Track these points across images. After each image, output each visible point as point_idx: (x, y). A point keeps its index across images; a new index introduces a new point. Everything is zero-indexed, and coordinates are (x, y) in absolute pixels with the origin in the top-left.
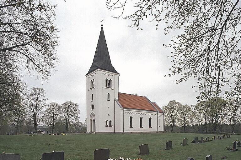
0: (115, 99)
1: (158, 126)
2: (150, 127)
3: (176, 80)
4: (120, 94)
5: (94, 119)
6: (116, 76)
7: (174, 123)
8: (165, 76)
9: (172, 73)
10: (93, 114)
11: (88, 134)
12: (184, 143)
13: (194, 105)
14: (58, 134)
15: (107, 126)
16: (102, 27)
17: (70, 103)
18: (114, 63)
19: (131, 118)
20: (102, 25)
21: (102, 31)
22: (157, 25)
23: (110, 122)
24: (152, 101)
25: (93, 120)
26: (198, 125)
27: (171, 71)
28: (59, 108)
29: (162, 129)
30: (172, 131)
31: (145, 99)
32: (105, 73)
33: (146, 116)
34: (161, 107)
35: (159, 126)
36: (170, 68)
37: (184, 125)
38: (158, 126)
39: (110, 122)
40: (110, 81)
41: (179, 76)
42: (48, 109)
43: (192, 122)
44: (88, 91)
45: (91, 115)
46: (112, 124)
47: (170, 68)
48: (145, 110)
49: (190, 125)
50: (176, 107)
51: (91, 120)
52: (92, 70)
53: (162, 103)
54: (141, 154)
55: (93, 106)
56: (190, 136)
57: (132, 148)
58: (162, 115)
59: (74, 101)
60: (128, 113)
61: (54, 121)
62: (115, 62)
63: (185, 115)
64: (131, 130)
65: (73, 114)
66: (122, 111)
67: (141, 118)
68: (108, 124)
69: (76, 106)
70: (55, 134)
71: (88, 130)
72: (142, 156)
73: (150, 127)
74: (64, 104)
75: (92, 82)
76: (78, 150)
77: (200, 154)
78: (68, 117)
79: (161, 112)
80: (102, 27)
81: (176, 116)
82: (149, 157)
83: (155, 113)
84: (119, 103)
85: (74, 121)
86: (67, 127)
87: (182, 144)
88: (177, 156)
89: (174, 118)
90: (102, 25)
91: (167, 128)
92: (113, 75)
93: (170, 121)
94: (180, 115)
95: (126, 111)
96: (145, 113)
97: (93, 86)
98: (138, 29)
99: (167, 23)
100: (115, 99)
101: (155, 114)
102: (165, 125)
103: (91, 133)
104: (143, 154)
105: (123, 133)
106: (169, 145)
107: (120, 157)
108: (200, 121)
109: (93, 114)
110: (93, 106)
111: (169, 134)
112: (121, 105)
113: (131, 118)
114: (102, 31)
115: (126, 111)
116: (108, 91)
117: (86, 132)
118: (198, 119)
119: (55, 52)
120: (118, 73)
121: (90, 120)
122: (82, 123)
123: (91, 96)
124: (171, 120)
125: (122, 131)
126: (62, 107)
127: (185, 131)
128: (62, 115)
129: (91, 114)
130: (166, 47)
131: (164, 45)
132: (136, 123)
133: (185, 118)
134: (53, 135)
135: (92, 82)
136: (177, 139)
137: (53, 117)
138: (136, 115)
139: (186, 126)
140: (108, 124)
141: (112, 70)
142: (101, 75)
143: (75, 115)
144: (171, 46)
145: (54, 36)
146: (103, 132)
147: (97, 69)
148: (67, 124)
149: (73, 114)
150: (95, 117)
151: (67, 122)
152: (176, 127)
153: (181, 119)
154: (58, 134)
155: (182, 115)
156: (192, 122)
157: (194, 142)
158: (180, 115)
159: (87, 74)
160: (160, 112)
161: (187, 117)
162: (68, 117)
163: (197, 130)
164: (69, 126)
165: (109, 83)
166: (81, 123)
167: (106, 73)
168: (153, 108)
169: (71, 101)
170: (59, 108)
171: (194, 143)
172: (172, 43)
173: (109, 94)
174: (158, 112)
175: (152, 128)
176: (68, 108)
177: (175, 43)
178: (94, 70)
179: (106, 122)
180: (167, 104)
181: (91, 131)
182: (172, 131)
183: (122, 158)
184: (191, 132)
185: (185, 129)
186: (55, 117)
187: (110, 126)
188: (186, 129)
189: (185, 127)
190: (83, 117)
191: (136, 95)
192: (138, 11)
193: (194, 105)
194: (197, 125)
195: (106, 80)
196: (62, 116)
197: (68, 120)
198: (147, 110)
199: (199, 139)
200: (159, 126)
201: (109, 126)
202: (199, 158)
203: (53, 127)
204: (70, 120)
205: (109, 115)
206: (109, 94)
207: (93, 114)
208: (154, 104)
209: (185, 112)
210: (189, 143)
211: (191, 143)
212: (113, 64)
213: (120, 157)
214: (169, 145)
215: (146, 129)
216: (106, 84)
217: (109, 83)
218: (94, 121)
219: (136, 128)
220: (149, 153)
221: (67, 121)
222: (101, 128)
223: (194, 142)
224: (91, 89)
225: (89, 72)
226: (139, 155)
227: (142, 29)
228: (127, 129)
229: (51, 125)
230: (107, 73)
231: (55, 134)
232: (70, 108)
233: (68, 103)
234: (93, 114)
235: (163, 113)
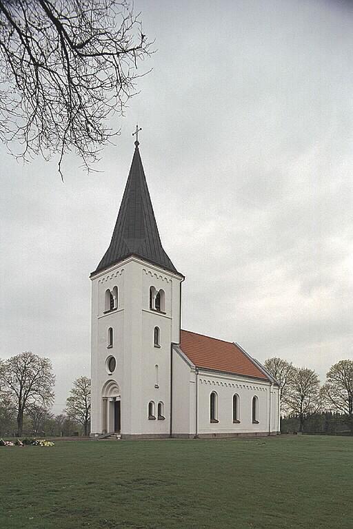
5: (115, 398)
6: (176, 282)
10: (112, 384)
15: (151, 418)
16: (137, 149)
17: (28, 357)
18: (169, 244)
20: (137, 143)
32: (148, 270)
39: (159, 405)
44: (96, 320)
45: (104, 387)
46: (166, 413)
51: (105, 399)
52: (109, 261)
59: (41, 355)
62: (171, 240)
64: (237, 429)
68: (155, 413)
69: (44, 364)
71: (96, 428)
75: (111, 298)
80: (137, 149)
83: (265, 386)
84: (180, 351)
90: (137, 143)
92: (169, 278)
95: (204, 377)
100: (172, 344)
102: (281, 417)
103: (105, 436)
105: (196, 437)
115: (203, 378)
116: (156, 319)
125: (192, 432)
126: (8, 366)
132: (224, 409)
134: (12, 444)
135: (111, 298)
138: (226, 387)
140: (155, 413)
141: (165, 264)
159: (93, 274)
164: (28, 419)
165: (157, 300)
169: (33, 353)
174: (271, 383)
179: (150, 405)
181: (106, 431)
187: (161, 418)
197: (25, 400)
198: (239, 375)
201: (157, 417)
204: (31, 400)
206: (157, 329)
212: (166, 246)
215: (246, 427)
216: (151, 305)
217: (157, 300)
218: (117, 405)
219: (225, 426)
222: (136, 424)
224: (105, 313)
225: (101, 268)
228: (206, 428)
230: (153, 272)
231: (17, 444)
233: (25, 356)
234: (114, 386)
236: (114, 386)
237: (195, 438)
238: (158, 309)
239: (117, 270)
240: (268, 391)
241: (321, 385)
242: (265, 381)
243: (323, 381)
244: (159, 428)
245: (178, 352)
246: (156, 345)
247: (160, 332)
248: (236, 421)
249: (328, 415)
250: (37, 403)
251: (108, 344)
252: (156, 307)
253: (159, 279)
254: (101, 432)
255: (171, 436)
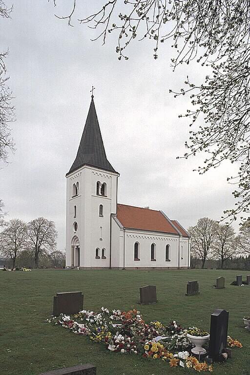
0: (111, 214)
1: (180, 258)
2: (167, 259)
3: (199, 167)
4: (119, 206)
5: (78, 246)
6: (114, 177)
7: (206, 254)
8: (178, 158)
9: (189, 151)
11: (68, 270)
12: (219, 285)
13: (230, 211)
14: (17, 269)
15: (97, 257)
16: (92, 100)
17: (42, 221)
19: (136, 245)
20: (93, 97)
21: (92, 105)
22: (156, 50)
23: (103, 250)
24: (171, 218)
25: (76, 247)
26: (245, 257)
27: (188, 147)
28: (25, 229)
29: (186, 263)
30: (203, 266)
31: (159, 214)
33: (161, 241)
34: (186, 228)
35: (182, 259)
36: (186, 142)
37: (222, 256)
38: (180, 258)
39: (103, 250)
40: (104, 186)
41: (203, 156)
42: (7, 231)
43: (234, 253)
44: (68, 201)
45: (72, 240)
46: (107, 254)
47: (186, 142)
48: (159, 232)
49: (232, 258)
50: (209, 229)
51: (73, 247)
52: (74, 169)
53: (187, 224)
54: (141, 302)
55: (76, 224)
56: (230, 275)
57: (129, 293)
58: (176, 238)
59: (49, 218)
60: (133, 237)
61: (15, 250)
63: (224, 241)
64: (137, 264)
65: (47, 238)
66: (122, 233)
67: (153, 246)
68: (100, 255)
70: (12, 270)
71: (68, 264)
72: (143, 307)
73: (167, 259)
74: (33, 223)
75: (76, 187)
76: (37, 294)
77: (243, 303)
78: (38, 243)
79: (186, 236)
80: (92, 100)
81: (209, 243)
82: (156, 308)
83: (176, 238)
84: (117, 220)
85: (48, 250)
86: (36, 259)
87: (215, 286)
88: (205, 307)
89: (206, 246)
90: (93, 97)
91: (194, 262)
92: (109, 175)
93: (200, 251)
94: (215, 240)
95: (129, 233)
96: (167, 237)
97: (77, 194)
98: (120, 59)
99: (176, 47)
100: (111, 214)
101: (175, 239)
102: (191, 257)
103: (73, 268)
104: (146, 303)
105: (124, 269)
106: (193, 288)
107: (102, 308)
108: (247, 250)
109: (75, 238)
110: (76, 224)
111: (197, 271)
112: (120, 224)
113: (136, 245)
114: (92, 105)
115: (128, 234)
116: (100, 200)
117: (64, 267)
118: (243, 247)
119: (7, 132)
120: (117, 173)
121: (71, 247)
122: (62, 254)
123: (74, 208)
124: (201, 249)
125: (121, 266)
127: (224, 267)
128: (28, 240)
129: (73, 238)
130: (175, 97)
131: (170, 91)
132: (160, 253)
133: (223, 245)
134: (10, 270)
135: (76, 187)
136: (206, 279)
137: (15, 243)
138: (146, 240)
139: (225, 259)
140: (100, 255)
141: (108, 168)
142: (90, 176)
143: (49, 240)
144: (184, 94)
145: (6, 105)
146: (91, 267)
147: (83, 165)
148: (36, 254)
149: (47, 238)
150: (79, 243)
151: (36, 250)
152: (210, 261)
153: (217, 247)
154: (17, 269)
155: (219, 241)
156: (234, 253)
157: (235, 284)
158: (215, 240)
159: (67, 174)
160: (183, 236)
161: (227, 244)
162: (38, 243)
163: (242, 265)
164: (40, 259)
165: (102, 189)
166: (61, 253)
167: (104, 174)
168: (170, 228)
170: (25, 229)
171: (235, 285)
172: (187, 87)
173: (101, 206)
175: (139, 260)
176: (38, 230)
177: (192, 88)
178: (78, 168)
179: (97, 250)
180: (195, 224)
181: (73, 265)
182: (203, 266)
183: (105, 310)
184: (233, 269)
185: (224, 264)
186: (17, 243)
187: (103, 257)
188: (225, 263)
189: (223, 260)
190: (61, 245)
191: (147, 209)
192: (110, 3)
193: (230, 211)
194: (243, 258)
195: (98, 184)
196: (29, 242)
198: (155, 232)
199: (245, 279)
200: (182, 259)
201: (101, 257)
202: (242, 310)
203: (15, 258)
205: (101, 239)
206: (101, 206)
207: (75, 238)
208: (174, 222)
209: (224, 237)
210: (227, 285)
211: (231, 284)
213: (102, 308)
214: (193, 288)
215: (160, 262)
216: (98, 192)
217: (102, 189)
218: (78, 249)
219: (145, 262)
220: (157, 301)
221: (38, 250)
222: (88, 261)
223: (235, 284)
226: (139, 304)
227: (128, 59)
228: (131, 263)
229: (11, 255)
231: (12, 270)
232: (41, 229)
235: (188, 237)
236: (77, 239)
237: (123, 269)
238: (103, 194)
239: (78, 173)
240: (178, 241)
241: (236, 235)
242: (176, 234)
243: (237, 231)
244: (103, 264)
245: (114, 219)
246: (101, 215)
247: (103, 208)
248: (153, 259)
249: (241, 258)
250: (46, 248)
251: (74, 215)
252: (101, 193)
253: (102, 176)
254: (70, 266)
255: (110, 268)
